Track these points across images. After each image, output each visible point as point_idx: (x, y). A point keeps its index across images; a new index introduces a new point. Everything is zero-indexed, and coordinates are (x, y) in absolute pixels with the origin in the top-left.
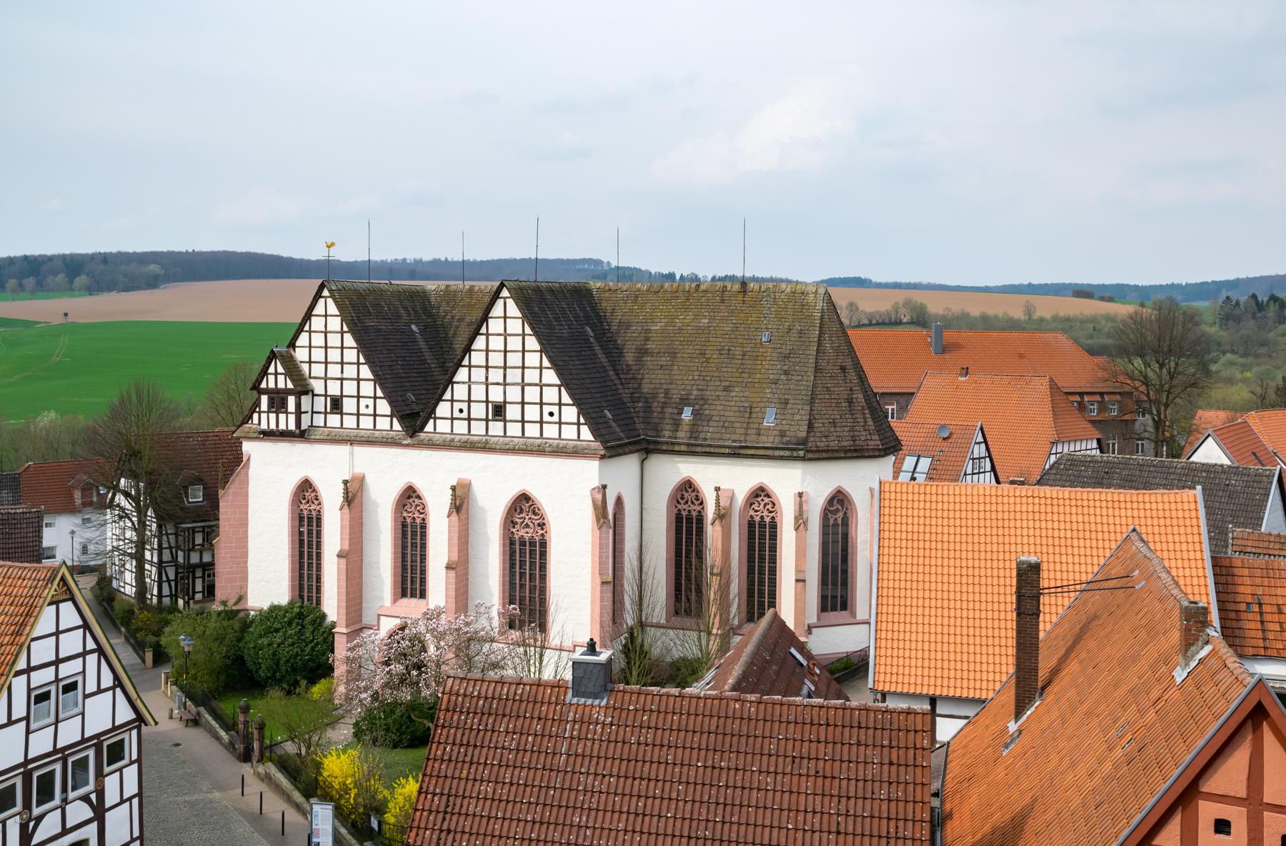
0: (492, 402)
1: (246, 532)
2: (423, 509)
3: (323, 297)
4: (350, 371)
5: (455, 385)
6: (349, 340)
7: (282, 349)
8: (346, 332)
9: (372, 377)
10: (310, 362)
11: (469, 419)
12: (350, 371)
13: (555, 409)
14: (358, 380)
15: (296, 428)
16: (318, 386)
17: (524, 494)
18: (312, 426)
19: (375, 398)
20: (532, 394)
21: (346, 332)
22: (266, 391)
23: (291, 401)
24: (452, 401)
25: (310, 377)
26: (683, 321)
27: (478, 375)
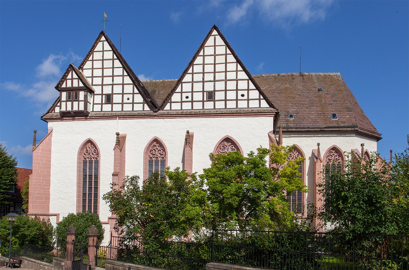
0: (206, 92)
1: (49, 172)
3: (102, 41)
8: (115, 59)
11: (192, 101)
14: (123, 84)
16: (97, 90)
19: (133, 94)
20: (231, 85)
21: (115, 59)
22: (66, 90)
23: (82, 94)
24: (182, 92)
25: (92, 85)
27: (198, 77)
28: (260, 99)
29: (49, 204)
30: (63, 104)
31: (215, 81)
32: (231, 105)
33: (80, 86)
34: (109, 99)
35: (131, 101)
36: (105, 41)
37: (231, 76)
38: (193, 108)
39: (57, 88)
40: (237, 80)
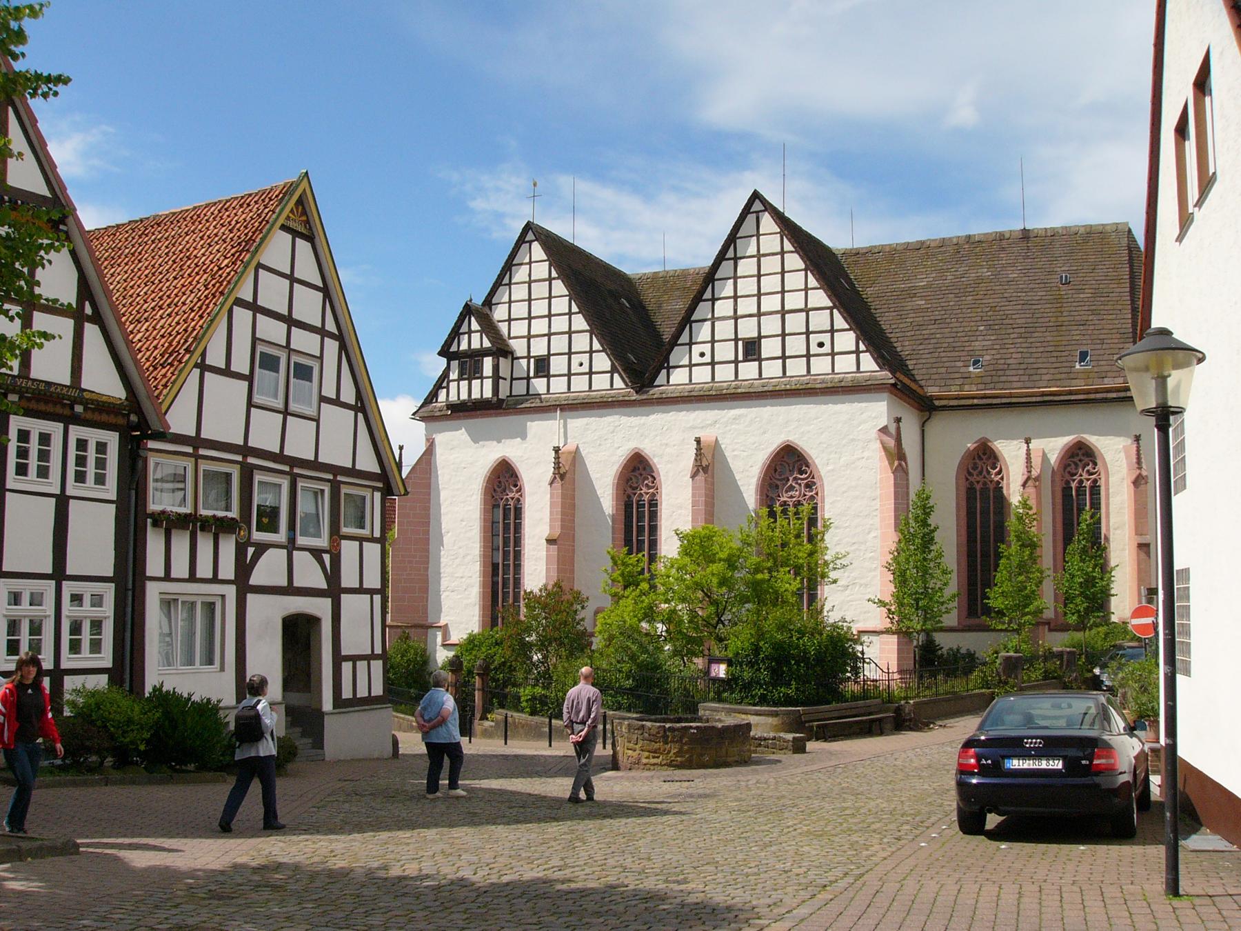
0: (743, 339)
3: (527, 242)
4: (560, 324)
5: (693, 324)
6: (559, 287)
8: (554, 279)
9: (588, 328)
10: (510, 320)
11: (713, 363)
12: (560, 324)
13: (826, 338)
15: (493, 395)
16: (519, 347)
17: (788, 446)
18: (511, 395)
20: (795, 323)
23: (488, 362)
25: (510, 338)
26: (955, 273)
28: (857, 352)
29: (427, 602)
30: (453, 386)
31: (549, 335)
32: (796, 368)
33: (484, 346)
34: (542, 368)
35: (585, 368)
36: (534, 241)
40: (807, 310)
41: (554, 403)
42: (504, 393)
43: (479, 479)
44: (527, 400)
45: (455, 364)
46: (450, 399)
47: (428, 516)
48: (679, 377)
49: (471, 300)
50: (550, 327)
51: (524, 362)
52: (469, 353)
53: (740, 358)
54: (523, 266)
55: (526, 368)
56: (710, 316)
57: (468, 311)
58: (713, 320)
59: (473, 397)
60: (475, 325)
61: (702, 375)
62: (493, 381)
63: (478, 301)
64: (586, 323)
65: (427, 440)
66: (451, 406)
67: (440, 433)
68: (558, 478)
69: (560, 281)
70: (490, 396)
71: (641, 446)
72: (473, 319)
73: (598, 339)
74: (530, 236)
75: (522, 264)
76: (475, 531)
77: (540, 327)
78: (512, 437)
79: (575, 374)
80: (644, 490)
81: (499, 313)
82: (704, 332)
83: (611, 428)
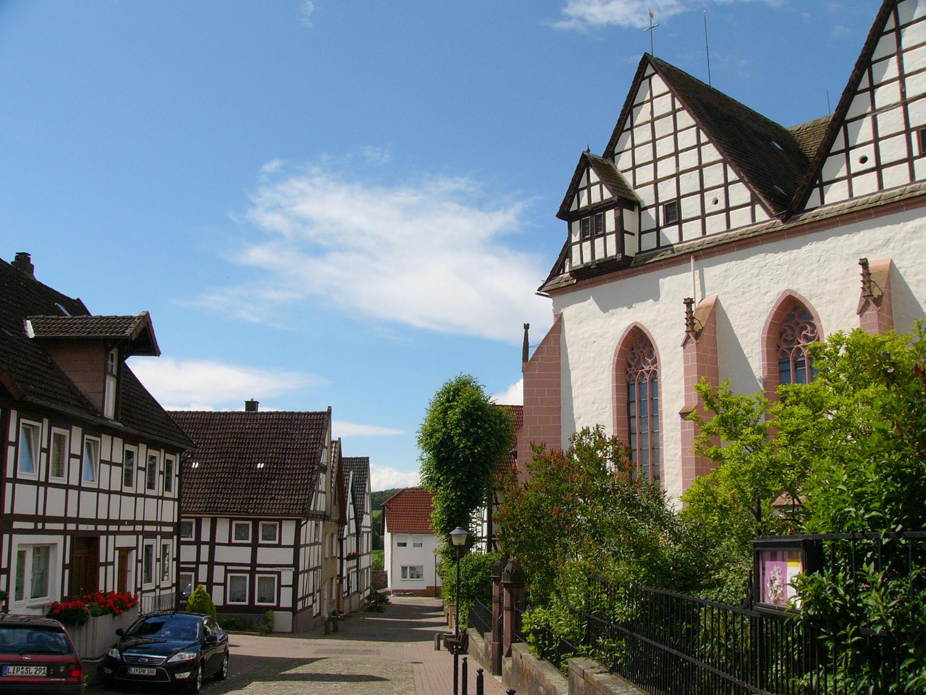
2: (812, 332)
6: (685, 119)
7: (598, 151)
9: (720, 157)
15: (618, 252)
16: (645, 195)
18: (640, 252)
25: (635, 187)
31: (677, 175)
34: (672, 212)
36: (653, 74)
37: (689, 160)
38: (883, 188)
39: (565, 214)
41: (687, 251)
42: (631, 249)
43: (610, 353)
44: (657, 254)
45: (576, 225)
46: (574, 265)
47: (559, 401)
48: (836, 194)
49: (588, 151)
50: (677, 165)
51: (652, 212)
52: (590, 209)
53: (916, 152)
54: (644, 105)
55: (654, 218)
56: (869, 110)
57: (586, 162)
58: (875, 113)
59: (597, 258)
60: (594, 178)
61: (866, 186)
62: (616, 236)
63: (598, 151)
64: (717, 153)
65: (556, 316)
66: (575, 273)
67: (568, 306)
68: (692, 338)
69: (685, 112)
70: (614, 253)
71: (794, 287)
72: (591, 171)
73: (704, 132)
74: (649, 70)
75: (642, 103)
76: (608, 414)
77: (667, 168)
78: (644, 299)
79: (710, 214)
80: (803, 342)
81: (623, 162)
82: (864, 131)
83: (756, 271)
